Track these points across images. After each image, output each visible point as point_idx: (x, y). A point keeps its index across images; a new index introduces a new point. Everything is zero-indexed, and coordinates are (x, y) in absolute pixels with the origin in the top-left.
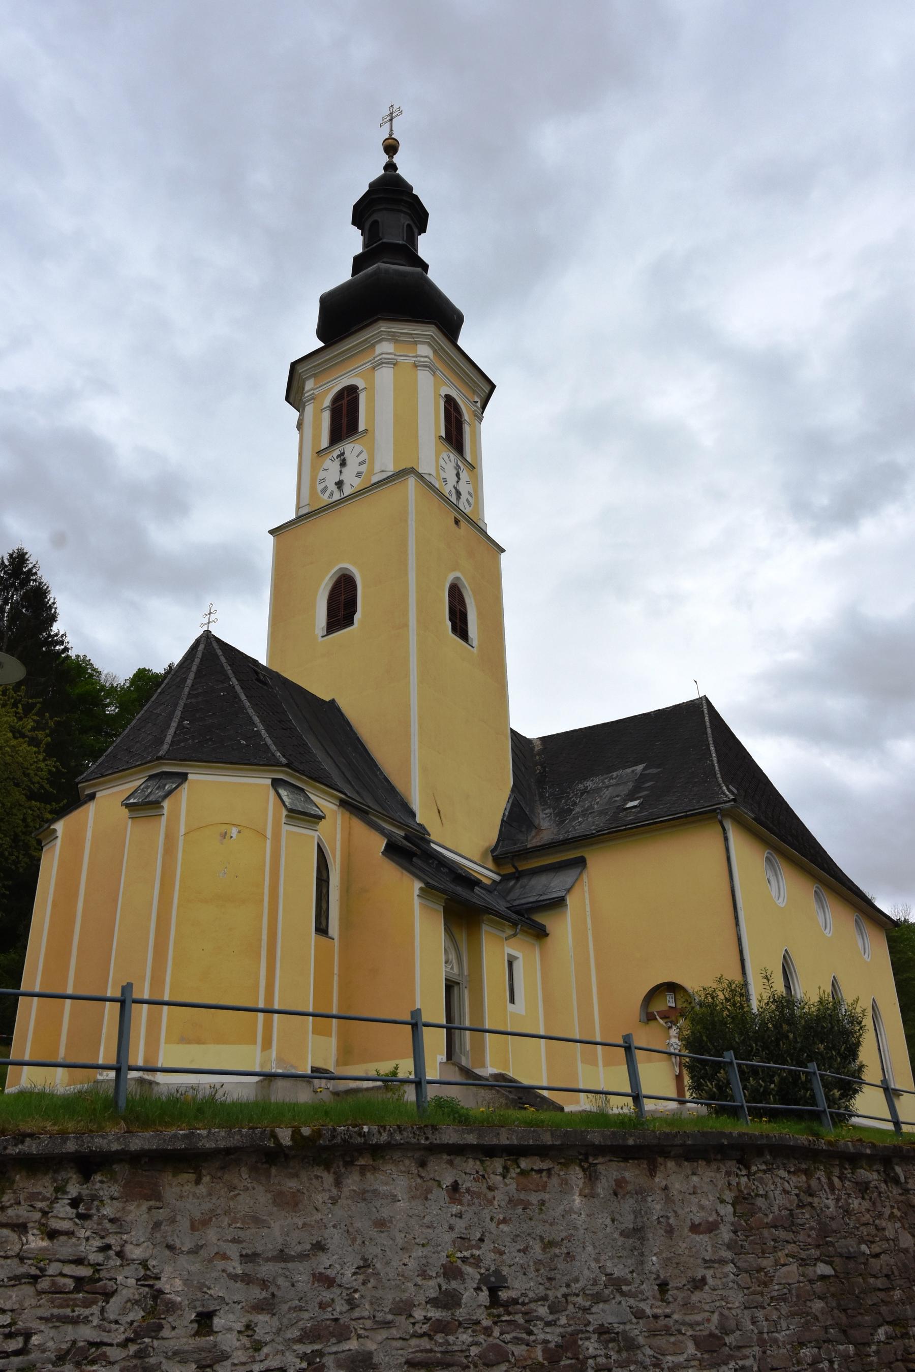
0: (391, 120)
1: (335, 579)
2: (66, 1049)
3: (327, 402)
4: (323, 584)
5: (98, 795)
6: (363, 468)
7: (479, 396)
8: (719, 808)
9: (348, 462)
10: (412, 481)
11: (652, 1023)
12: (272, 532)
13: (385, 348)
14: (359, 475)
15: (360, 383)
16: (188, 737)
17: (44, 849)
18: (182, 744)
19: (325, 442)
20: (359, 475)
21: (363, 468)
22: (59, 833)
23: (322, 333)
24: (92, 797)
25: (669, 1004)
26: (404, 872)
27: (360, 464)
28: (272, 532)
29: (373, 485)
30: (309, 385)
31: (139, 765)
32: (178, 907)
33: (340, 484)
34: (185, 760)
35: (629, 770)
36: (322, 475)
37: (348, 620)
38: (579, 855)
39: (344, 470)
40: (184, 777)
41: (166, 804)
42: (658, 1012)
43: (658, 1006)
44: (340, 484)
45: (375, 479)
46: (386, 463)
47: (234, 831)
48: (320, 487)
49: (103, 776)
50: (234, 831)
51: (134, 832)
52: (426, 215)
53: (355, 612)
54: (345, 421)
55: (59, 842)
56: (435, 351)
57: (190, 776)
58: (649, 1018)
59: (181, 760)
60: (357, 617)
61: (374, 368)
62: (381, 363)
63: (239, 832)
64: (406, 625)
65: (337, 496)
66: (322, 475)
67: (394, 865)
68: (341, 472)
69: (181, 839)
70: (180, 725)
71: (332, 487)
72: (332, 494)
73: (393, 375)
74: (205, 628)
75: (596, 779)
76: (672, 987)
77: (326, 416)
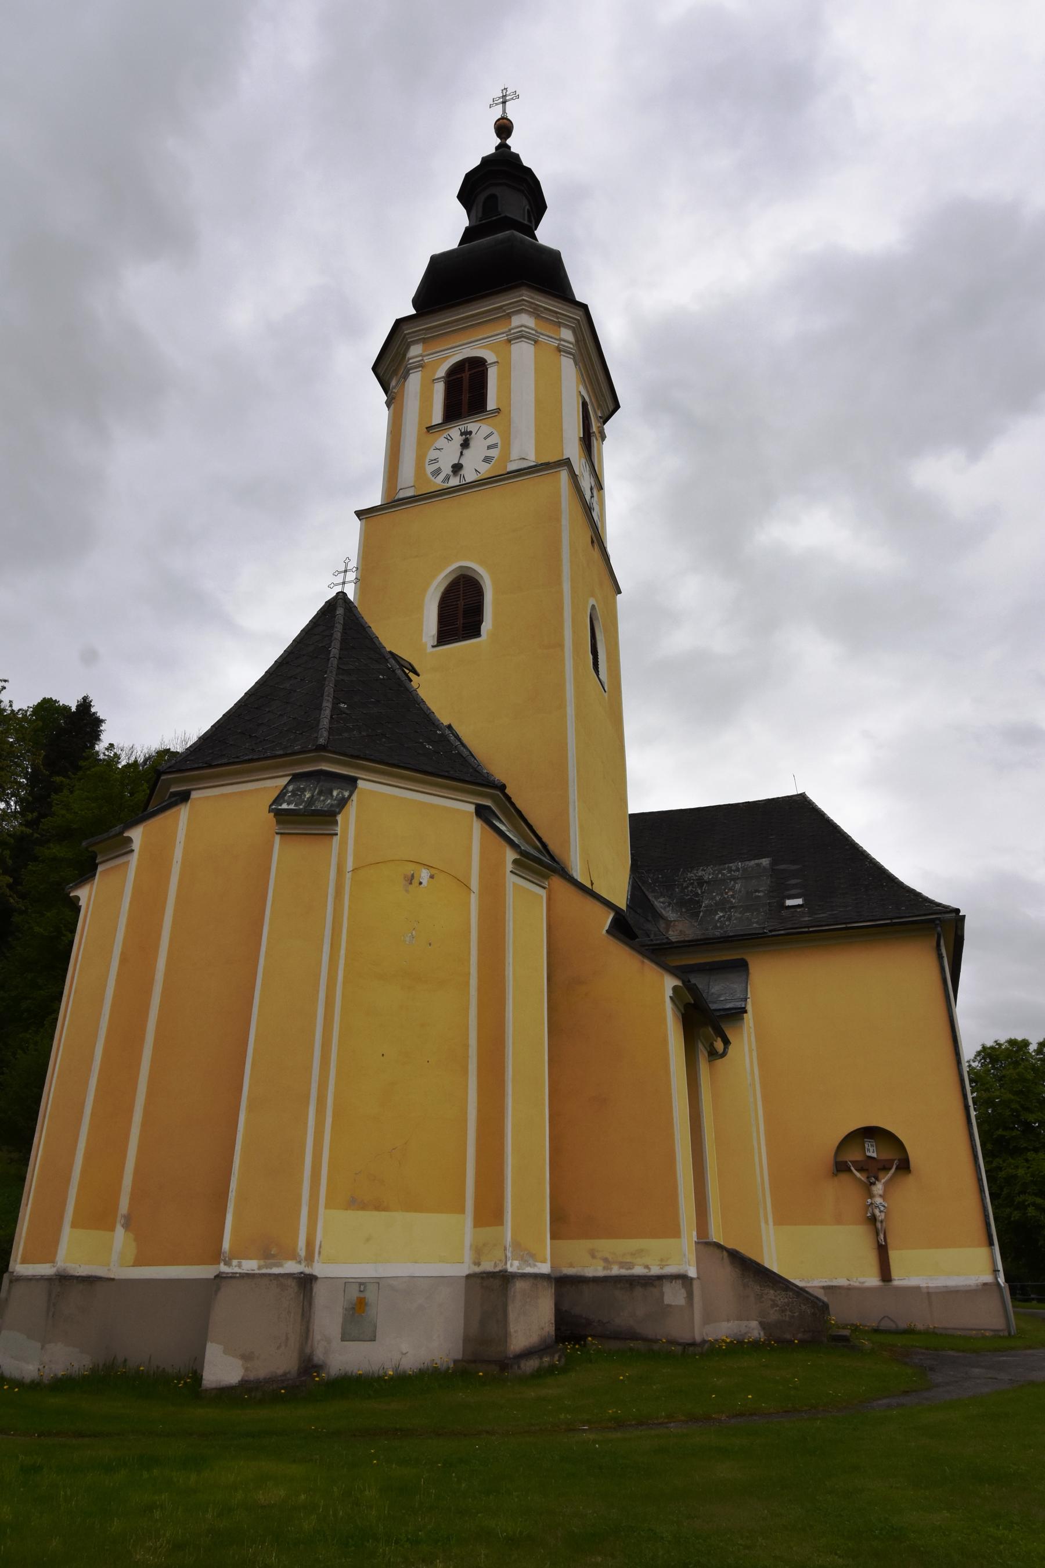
0: (504, 103)
1: (450, 579)
2: (132, 1199)
3: (442, 371)
4: (435, 583)
5: (194, 795)
6: (494, 453)
7: (602, 412)
8: (939, 919)
9: (472, 443)
10: (564, 474)
11: (844, 1177)
12: (359, 514)
13: (524, 320)
14: (487, 460)
15: (489, 357)
16: (350, 725)
17: (100, 869)
18: (346, 735)
19: (437, 417)
20: (487, 460)
21: (494, 453)
22: (136, 845)
23: (416, 302)
24: (184, 797)
25: (868, 1154)
26: (646, 961)
27: (489, 448)
28: (359, 514)
29: (508, 473)
30: (415, 351)
31: (281, 756)
32: (344, 983)
33: (457, 468)
34: (358, 757)
35: (753, 863)
36: (432, 454)
37: (473, 629)
38: (739, 957)
39: (465, 452)
40: (352, 781)
41: (339, 818)
42: (853, 1162)
43: (853, 1155)
44: (457, 468)
45: (512, 467)
46: (525, 450)
47: (424, 875)
48: (430, 469)
49: (210, 766)
50: (424, 875)
51: (284, 855)
52: (545, 207)
53: (481, 622)
54: (465, 397)
55: (134, 859)
56: (577, 341)
57: (360, 784)
58: (840, 1167)
59: (352, 756)
60: (486, 627)
61: (509, 341)
62: (521, 336)
63: (432, 877)
64: (561, 645)
65: (454, 482)
66: (432, 454)
67: (627, 948)
68: (461, 453)
69: (349, 876)
70: (335, 708)
71: (447, 470)
72: (447, 478)
73: (521, 363)
74: (339, 589)
75: (710, 869)
76: (870, 1133)
77: (439, 391)
